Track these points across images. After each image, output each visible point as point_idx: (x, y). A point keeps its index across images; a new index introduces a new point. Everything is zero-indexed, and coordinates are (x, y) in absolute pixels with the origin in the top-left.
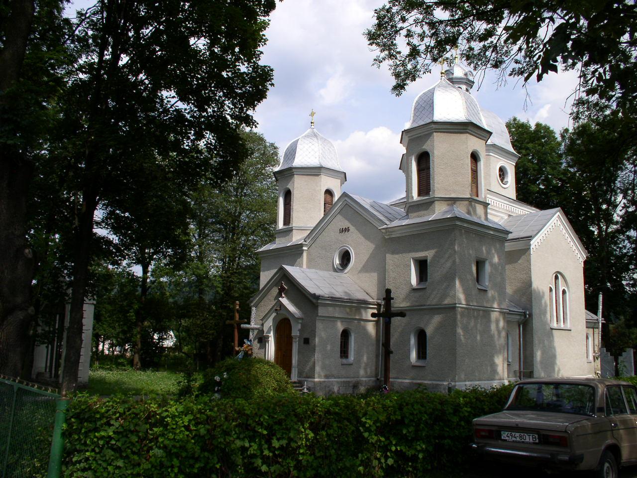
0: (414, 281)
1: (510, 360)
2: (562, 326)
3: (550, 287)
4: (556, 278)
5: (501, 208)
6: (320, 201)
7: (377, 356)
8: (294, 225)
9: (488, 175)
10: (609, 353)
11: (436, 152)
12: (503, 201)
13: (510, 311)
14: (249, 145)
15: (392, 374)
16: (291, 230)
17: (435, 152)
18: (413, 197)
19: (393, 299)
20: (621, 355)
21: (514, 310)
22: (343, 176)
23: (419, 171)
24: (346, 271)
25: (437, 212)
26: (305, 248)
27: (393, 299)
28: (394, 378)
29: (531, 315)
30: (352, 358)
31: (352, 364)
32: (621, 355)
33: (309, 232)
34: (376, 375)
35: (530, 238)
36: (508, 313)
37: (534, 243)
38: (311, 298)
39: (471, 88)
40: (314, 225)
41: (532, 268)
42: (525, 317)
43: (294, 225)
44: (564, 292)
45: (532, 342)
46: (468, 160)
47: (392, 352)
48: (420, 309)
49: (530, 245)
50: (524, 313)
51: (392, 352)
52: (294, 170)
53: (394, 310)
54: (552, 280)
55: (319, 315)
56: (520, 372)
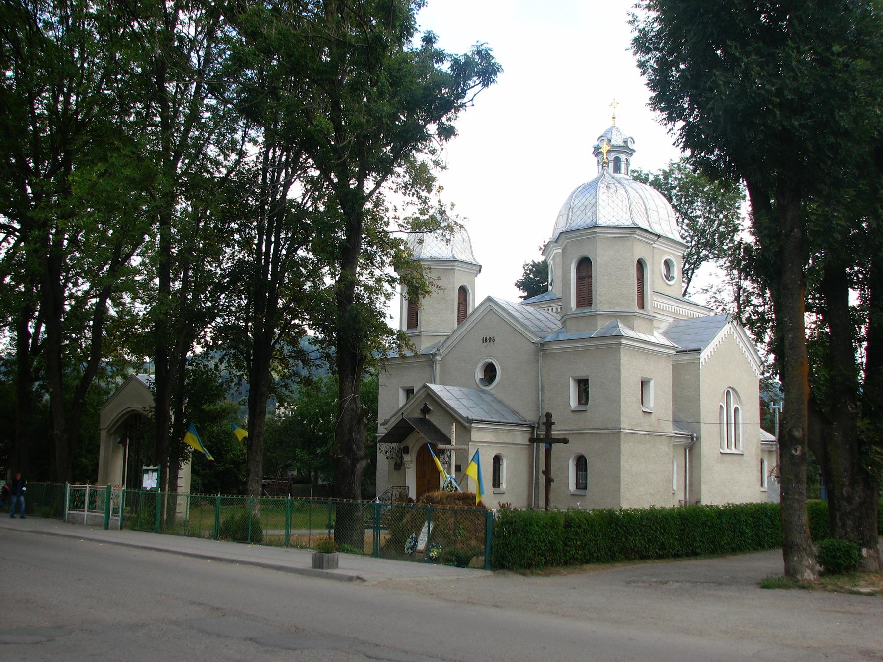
0: (573, 402)
1: (675, 489)
2: (733, 450)
3: (721, 406)
4: (728, 393)
6: (453, 301)
8: (423, 330)
12: (666, 301)
17: (598, 260)
18: (571, 309)
19: (554, 423)
21: (678, 432)
22: (479, 268)
23: (579, 278)
24: (762, 430)
25: (599, 327)
27: (554, 423)
29: (698, 438)
30: (504, 486)
31: (504, 493)
33: (445, 338)
35: (698, 350)
37: (703, 356)
41: (701, 385)
42: (692, 439)
43: (423, 330)
44: (736, 410)
47: (553, 481)
48: (579, 434)
50: (691, 436)
51: (553, 481)
53: (555, 434)
54: (723, 397)
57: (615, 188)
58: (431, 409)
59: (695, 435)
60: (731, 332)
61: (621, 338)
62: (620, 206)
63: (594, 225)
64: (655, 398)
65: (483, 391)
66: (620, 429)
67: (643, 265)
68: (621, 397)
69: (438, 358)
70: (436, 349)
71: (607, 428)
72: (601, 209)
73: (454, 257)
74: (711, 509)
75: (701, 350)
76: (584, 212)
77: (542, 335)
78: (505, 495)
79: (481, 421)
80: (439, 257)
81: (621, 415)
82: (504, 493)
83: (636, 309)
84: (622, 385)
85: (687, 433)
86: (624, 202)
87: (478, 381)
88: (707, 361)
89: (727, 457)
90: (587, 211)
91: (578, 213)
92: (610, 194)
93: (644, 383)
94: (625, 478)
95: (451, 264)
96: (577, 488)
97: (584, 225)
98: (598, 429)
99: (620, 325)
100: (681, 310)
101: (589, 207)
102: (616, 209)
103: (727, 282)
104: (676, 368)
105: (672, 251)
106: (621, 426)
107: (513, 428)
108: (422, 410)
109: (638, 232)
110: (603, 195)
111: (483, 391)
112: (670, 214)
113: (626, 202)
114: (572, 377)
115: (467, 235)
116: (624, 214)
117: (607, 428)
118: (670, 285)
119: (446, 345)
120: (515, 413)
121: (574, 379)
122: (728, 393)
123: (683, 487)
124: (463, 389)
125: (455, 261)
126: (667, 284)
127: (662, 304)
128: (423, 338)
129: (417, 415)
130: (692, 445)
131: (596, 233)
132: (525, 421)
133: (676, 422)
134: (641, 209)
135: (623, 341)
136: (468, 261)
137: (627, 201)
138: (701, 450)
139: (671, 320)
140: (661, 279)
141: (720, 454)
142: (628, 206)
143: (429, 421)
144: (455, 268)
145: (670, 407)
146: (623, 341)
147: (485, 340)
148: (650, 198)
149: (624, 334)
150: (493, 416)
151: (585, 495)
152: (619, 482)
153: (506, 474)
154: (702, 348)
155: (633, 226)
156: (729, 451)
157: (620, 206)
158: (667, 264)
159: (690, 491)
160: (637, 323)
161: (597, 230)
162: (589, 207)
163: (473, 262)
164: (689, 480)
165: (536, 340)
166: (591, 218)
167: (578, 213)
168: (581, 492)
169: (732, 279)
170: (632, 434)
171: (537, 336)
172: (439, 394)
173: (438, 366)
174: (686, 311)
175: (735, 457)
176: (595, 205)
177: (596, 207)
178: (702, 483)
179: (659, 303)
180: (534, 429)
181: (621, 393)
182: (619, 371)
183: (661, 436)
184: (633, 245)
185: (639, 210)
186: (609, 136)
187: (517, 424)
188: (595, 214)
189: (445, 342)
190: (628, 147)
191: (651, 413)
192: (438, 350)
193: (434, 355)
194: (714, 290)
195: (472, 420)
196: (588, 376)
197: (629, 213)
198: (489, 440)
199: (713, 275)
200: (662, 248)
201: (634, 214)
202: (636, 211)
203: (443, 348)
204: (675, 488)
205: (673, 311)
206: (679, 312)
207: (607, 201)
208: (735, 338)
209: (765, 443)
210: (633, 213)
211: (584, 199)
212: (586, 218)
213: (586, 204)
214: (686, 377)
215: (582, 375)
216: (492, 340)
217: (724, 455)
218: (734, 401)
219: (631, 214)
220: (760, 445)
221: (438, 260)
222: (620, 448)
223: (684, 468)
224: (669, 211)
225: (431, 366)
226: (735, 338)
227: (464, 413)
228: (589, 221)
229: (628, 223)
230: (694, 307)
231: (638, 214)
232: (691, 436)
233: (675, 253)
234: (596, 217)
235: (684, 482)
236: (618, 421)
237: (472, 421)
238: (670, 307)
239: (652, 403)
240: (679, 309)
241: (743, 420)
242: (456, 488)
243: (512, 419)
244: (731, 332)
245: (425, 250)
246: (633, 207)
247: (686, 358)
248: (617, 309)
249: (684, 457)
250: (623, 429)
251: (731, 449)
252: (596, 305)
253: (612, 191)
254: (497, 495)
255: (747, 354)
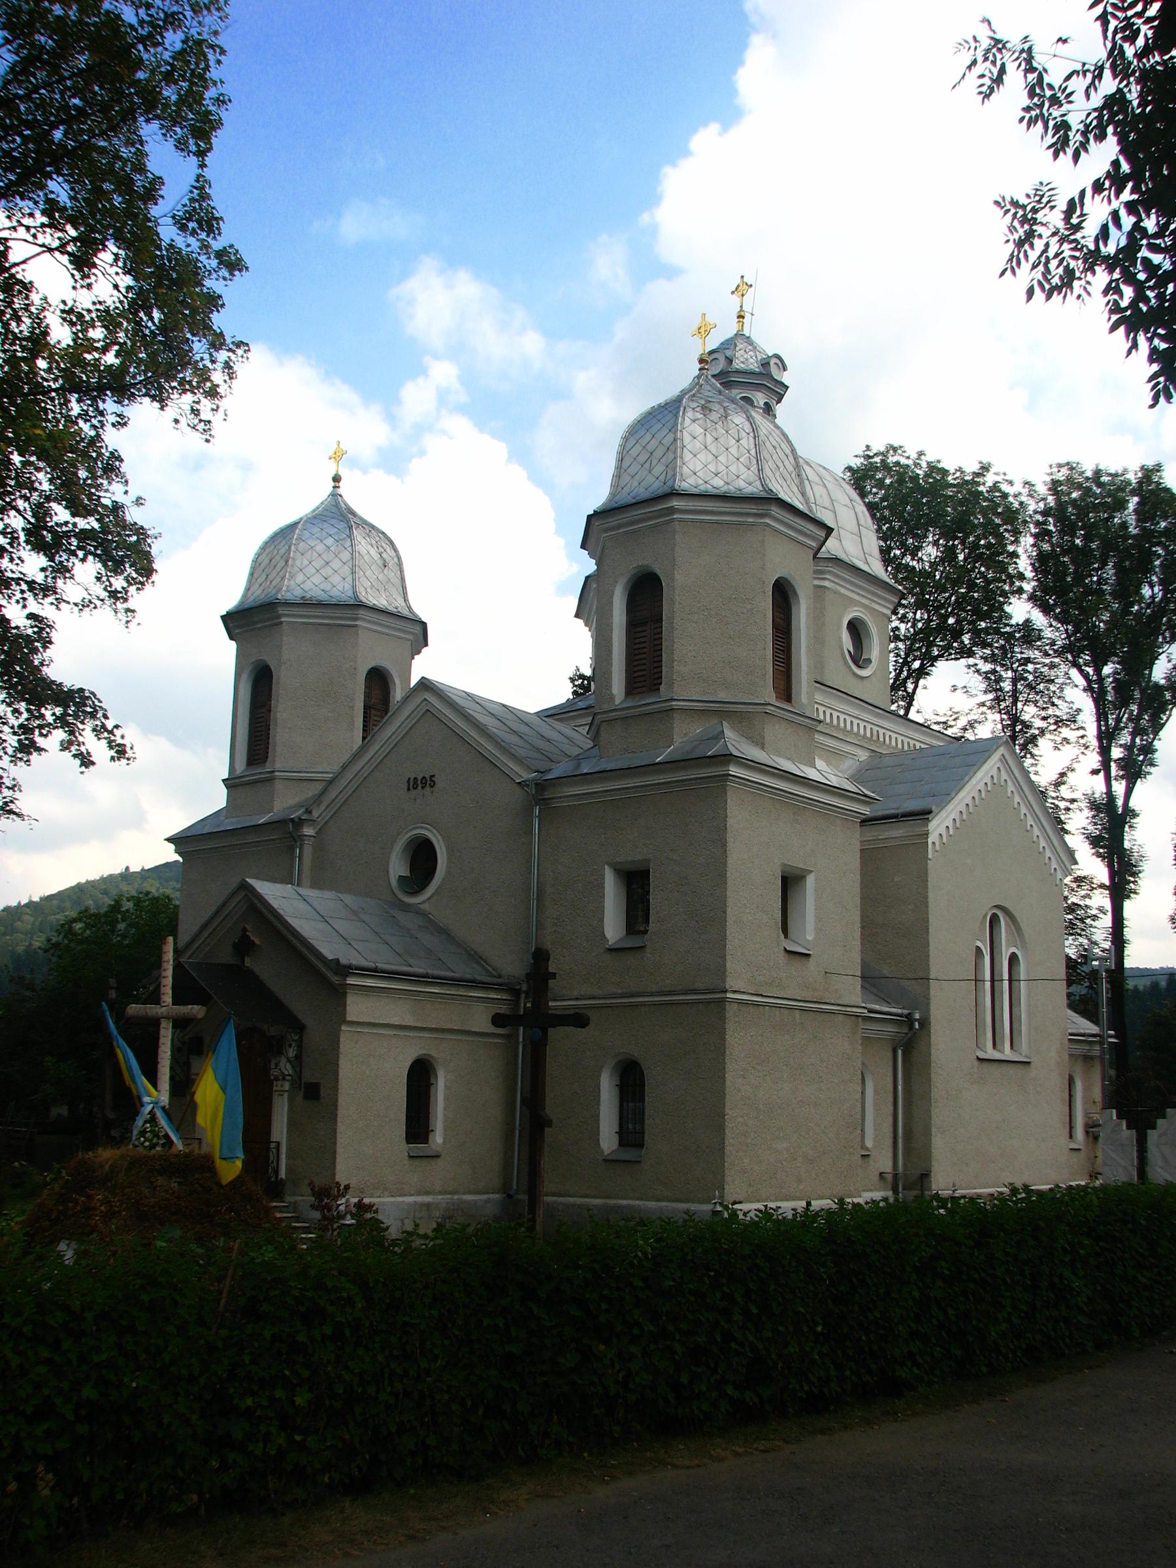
0: (613, 927)
2: (1007, 1053)
3: (978, 948)
4: (994, 920)
5: (844, 730)
7: (508, 1135)
8: (278, 766)
9: (818, 640)
10: (1124, 1123)
11: (679, 577)
12: (856, 712)
13: (870, 1011)
14: (753, 19)
15: (549, 1183)
16: (270, 780)
17: (677, 576)
18: (612, 697)
19: (127, 868)
20: (1154, 1127)
21: (877, 1007)
23: (633, 625)
24: (1070, 1013)
25: (678, 740)
26: (308, 831)
27: (553, 976)
28: (554, 1195)
29: (925, 1023)
30: (438, 1138)
32: (1154, 1127)
34: (505, 1188)
35: (925, 814)
36: (866, 1019)
37: (938, 827)
38: (329, 974)
39: (779, 401)
40: (336, 768)
42: (911, 1026)
43: (278, 766)
44: (1013, 959)
45: (927, 1096)
46: (766, 604)
47: (549, 1123)
49: (927, 834)
50: (909, 1016)
51: (549, 1123)
52: (281, 610)
53: (556, 1008)
54: (982, 929)
55: (349, 1019)
56: (895, 1176)
57: (722, 411)
58: (257, 942)
59: (917, 1016)
60: (999, 779)
61: (727, 763)
62: (733, 451)
63: (666, 489)
64: (819, 919)
65: (406, 908)
66: (726, 991)
67: (790, 594)
68: (729, 910)
69: (308, 831)
70: (303, 810)
71: (695, 991)
72: (687, 456)
73: (356, 597)
74: (950, 1212)
75: (930, 812)
76: (647, 465)
77: (542, 765)
78: (440, 1162)
79: (375, 970)
80: (323, 597)
81: (728, 957)
82: (438, 1156)
83: (768, 694)
84: (730, 881)
85: (899, 1011)
86: (744, 442)
87: (394, 882)
88: (945, 840)
89: (993, 1068)
90: (654, 463)
91: (632, 470)
92: (709, 424)
93: (790, 882)
94: (736, 1117)
95: (349, 613)
96: (621, 1144)
97: (644, 494)
98: (670, 993)
99: (728, 733)
100: (888, 733)
101: (659, 453)
102: (722, 459)
103: (988, 704)
104: (870, 858)
105: (864, 601)
106: (731, 983)
107: (462, 992)
108: (235, 945)
109: (775, 510)
110: (691, 427)
111: (406, 908)
112: (862, 522)
113: (747, 443)
114: (610, 865)
115: (393, 553)
116: (743, 469)
117: (695, 991)
118: (862, 678)
119: (326, 800)
120: (476, 957)
121: (615, 870)
122: (994, 920)
123: (889, 1141)
124: (348, 899)
125: (360, 606)
126: (855, 674)
127: (842, 717)
128: (279, 786)
129: (225, 956)
130: (910, 1039)
131: (672, 510)
132: (500, 977)
133: (871, 980)
134: (786, 462)
135: (734, 770)
136: (391, 609)
137: (752, 440)
138: (933, 1051)
139: (863, 755)
140: (842, 662)
141: (976, 1063)
142: (753, 452)
143: (250, 972)
144: (358, 623)
145: (856, 944)
146: (734, 770)
147: (414, 784)
148: (817, 479)
149: (735, 753)
150: (411, 961)
151: (639, 1162)
152: (721, 1128)
153: (445, 1109)
154: (934, 808)
155: (764, 495)
156: (997, 1055)
157: (733, 451)
158: (856, 628)
159: (908, 1151)
160: (774, 731)
161: (676, 503)
162: (659, 453)
163: (406, 612)
164: (904, 1126)
165: (526, 776)
166: (662, 478)
167: (632, 470)
168: (629, 1154)
169: (998, 700)
170: (757, 1005)
171: (529, 769)
172: (275, 904)
173: (308, 850)
174: (896, 738)
175: (1011, 1071)
176: (672, 448)
177: (675, 452)
178: (934, 1130)
179: (835, 714)
180: (518, 998)
181: (730, 903)
182: (724, 845)
183: (831, 1013)
184: (763, 542)
185: (781, 465)
186: (729, 353)
187: (474, 984)
188: (672, 467)
189: (324, 792)
190: (770, 376)
191: (808, 955)
192: (308, 811)
193: (299, 823)
194: (962, 722)
195: (350, 967)
196: (648, 861)
197: (754, 468)
198: (395, 1021)
199: (959, 692)
200: (843, 591)
201: (767, 472)
202: (773, 467)
203: (319, 805)
204: (869, 1143)
205: (868, 735)
206: (881, 739)
207: (700, 438)
208: (1009, 794)
209: (1076, 1039)
210: (766, 467)
211: (649, 436)
212: (651, 479)
213: (650, 447)
214: (897, 879)
215: (631, 855)
216: (428, 782)
217: (985, 1065)
218: (1008, 941)
219: (760, 470)
220: (1067, 1042)
221: (320, 605)
222: (724, 1040)
223: (891, 1096)
224: (860, 516)
225: (292, 849)
226: (1009, 794)
227: (329, 950)
228: (657, 484)
229: (754, 489)
230: (916, 731)
231: (777, 474)
232: (909, 1016)
233: (877, 607)
234: (675, 475)
235: (891, 1129)
236: (721, 972)
237: (345, 970)
238: (862, 724)
239: (808, 931)
240: (881, 731)
241: (1028, 972)
242: (167, 1136)
243: (463, 970)
244: (999, 779)
245: (292, 583)
246: (765, 454)
247: (897, 832)
248: (722, 696)
249: (890, 1069)
250: (735, 992)
251: (1002, 1051)
252: (671, 685)
253: (714, 416)
254: (417, 1162)
255: (1036, 831)
